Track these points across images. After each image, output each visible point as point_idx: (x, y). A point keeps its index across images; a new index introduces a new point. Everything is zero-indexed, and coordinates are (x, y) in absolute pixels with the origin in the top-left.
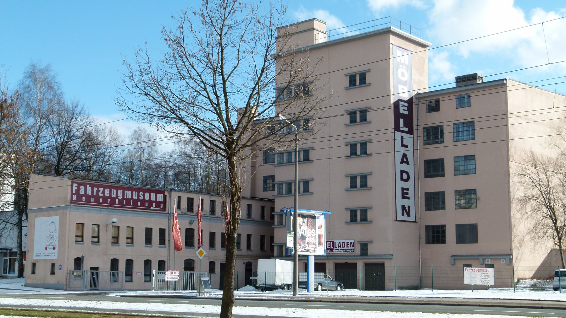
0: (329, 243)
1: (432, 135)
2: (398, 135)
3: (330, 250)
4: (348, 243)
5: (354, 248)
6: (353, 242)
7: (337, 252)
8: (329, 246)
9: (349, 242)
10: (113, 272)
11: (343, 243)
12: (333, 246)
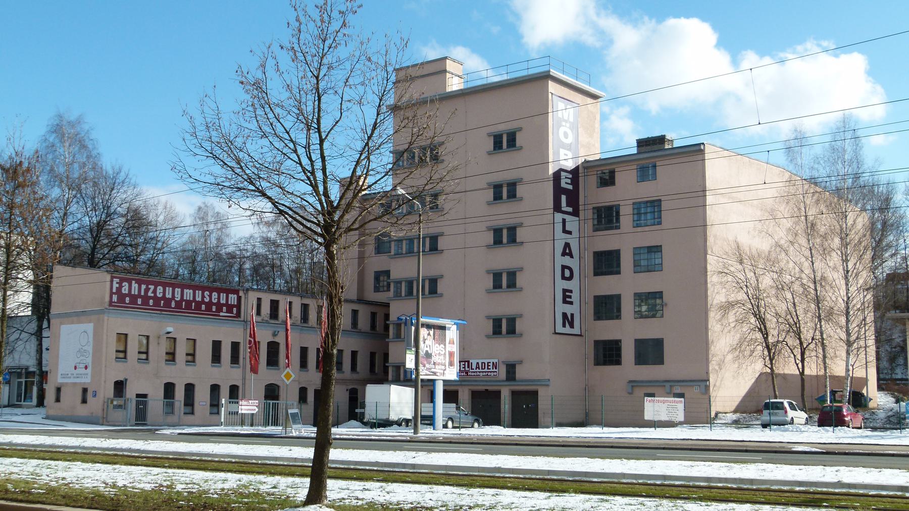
2: (559, 217)
5: (497, 370)
11: (482, 363)
12: (468, 367)
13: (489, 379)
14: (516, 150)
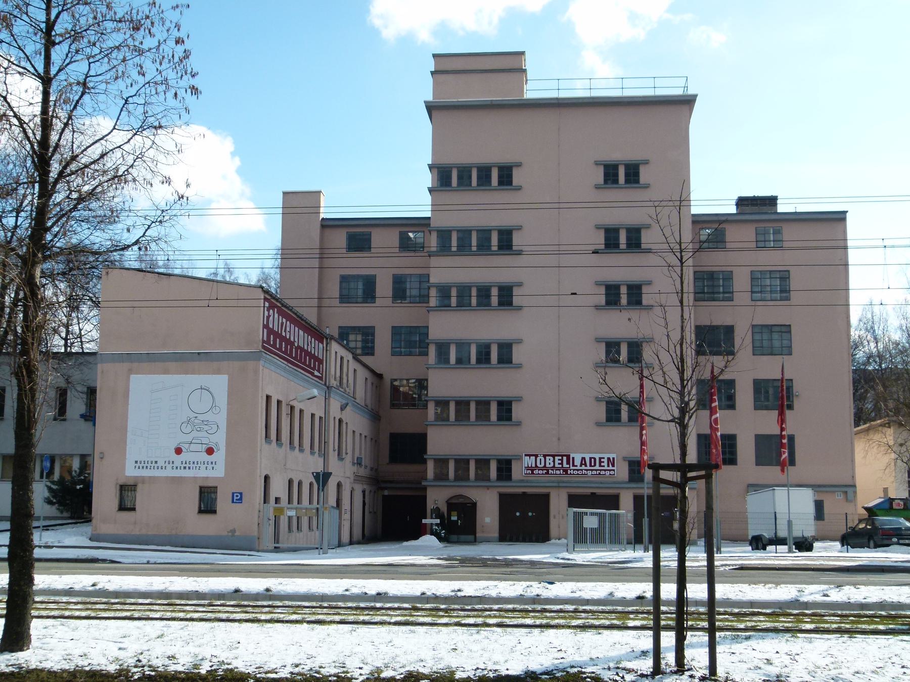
0: (560, 458)
1: (720, 286)
3: (561, 471)
4: (602, 460)
6: (614, 458)
7: (578, 474)
8: (559, 464)
9: (604, 458)
10: (575, 510)
11: (591, 459)
12: (568, 463)
13: (586, 479)
14: (490, 190)
